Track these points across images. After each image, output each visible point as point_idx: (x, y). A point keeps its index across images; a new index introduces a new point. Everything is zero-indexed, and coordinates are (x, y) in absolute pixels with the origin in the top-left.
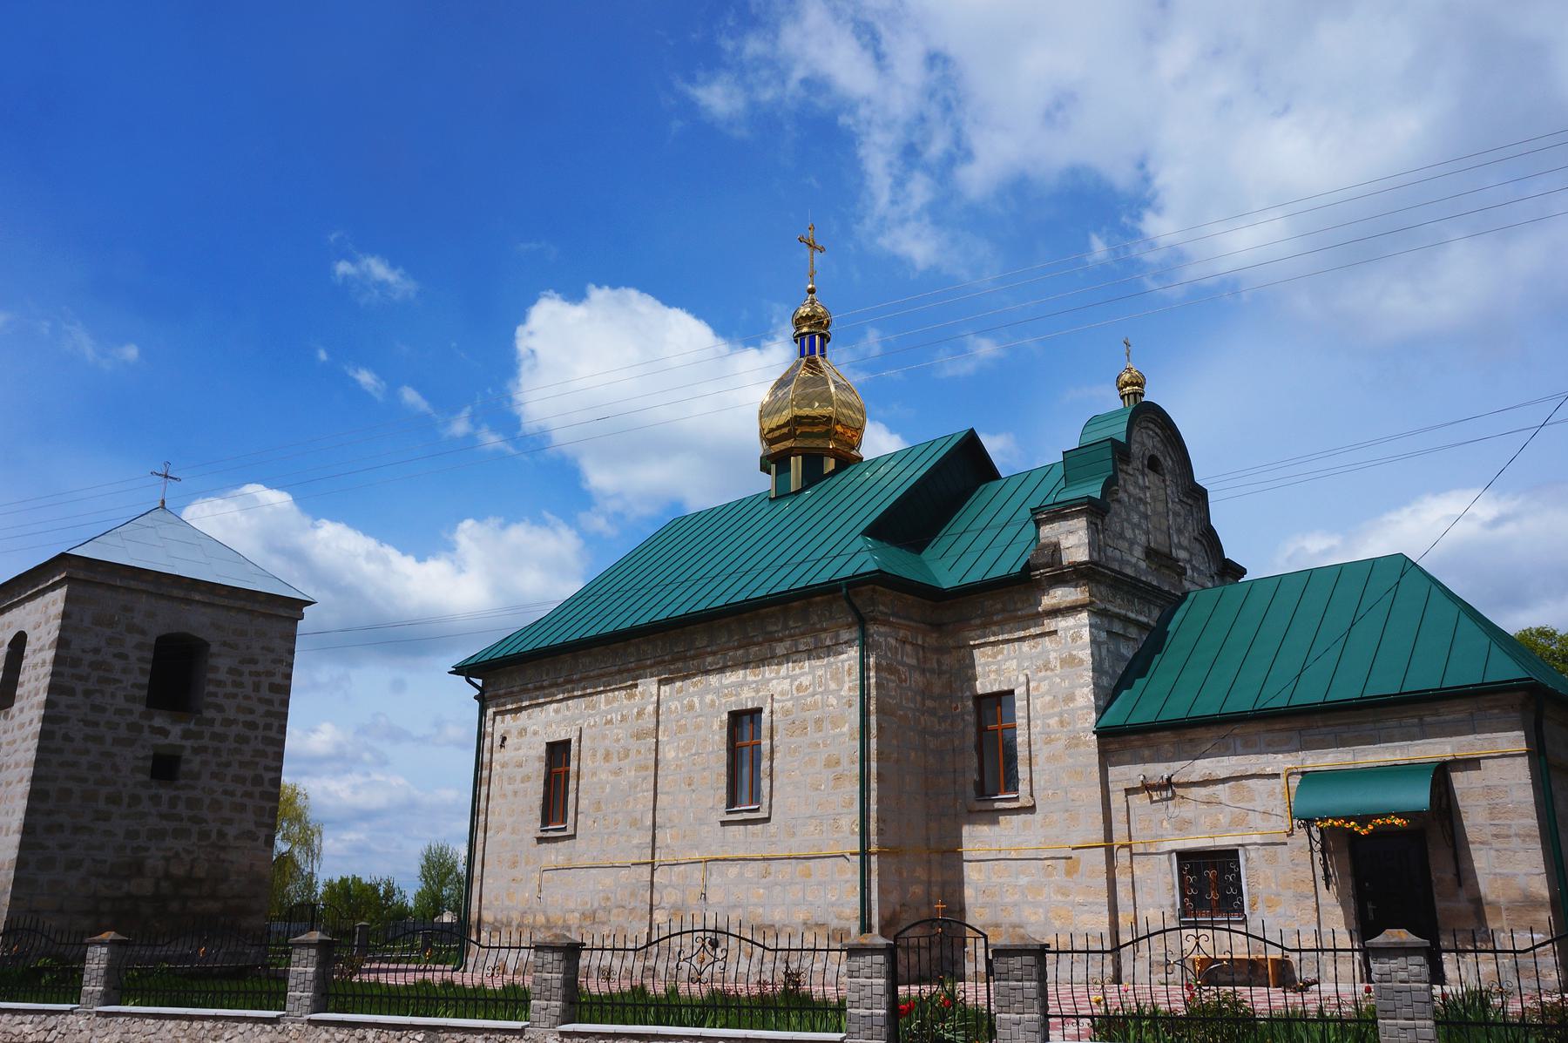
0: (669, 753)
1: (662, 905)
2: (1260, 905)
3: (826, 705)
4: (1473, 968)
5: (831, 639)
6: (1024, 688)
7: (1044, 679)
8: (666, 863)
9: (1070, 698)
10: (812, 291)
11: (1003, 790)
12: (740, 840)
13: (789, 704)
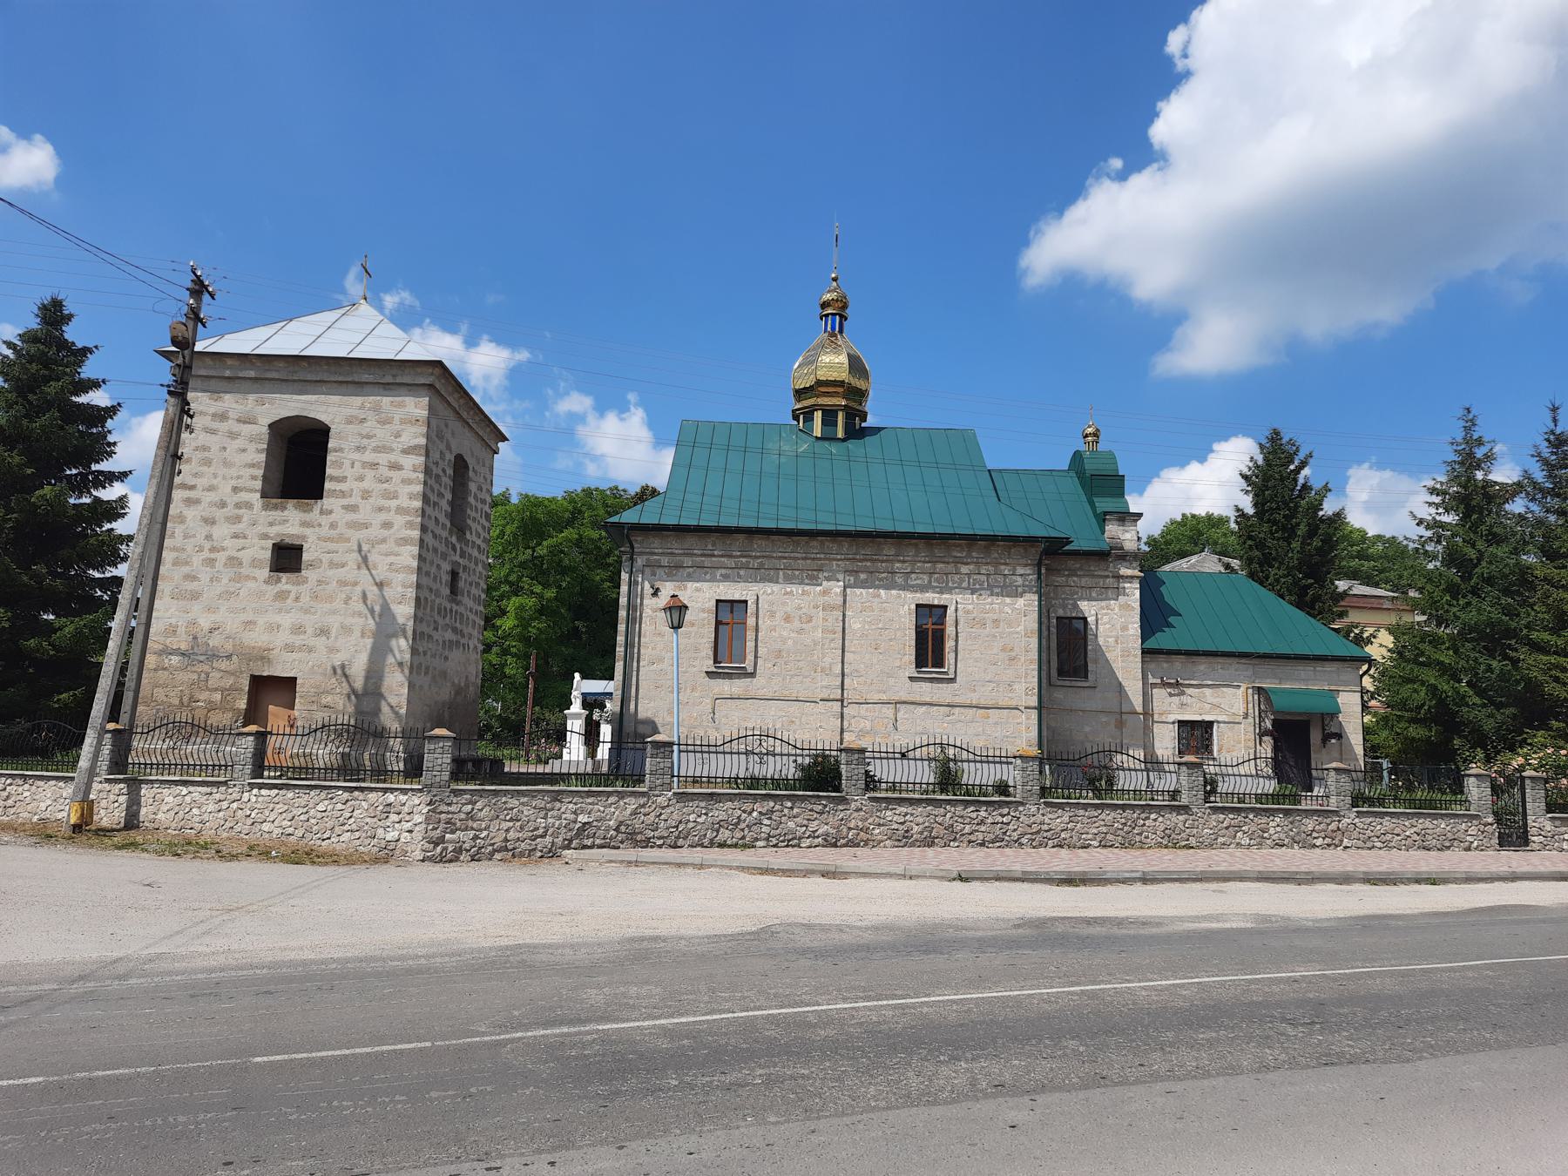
0: (854, 624)
1: (851, 729)
2: (1224, 751)
3: (1001, 611)
4: (567, 807)
5: (1009, 570)
6: (1094, 618)
7: (1106, 614)
8: (854, 701)
9: (1125, 628)
10: (835, 279)
11: (930, 664)
12: (925, 691)
13: (971, 607)
